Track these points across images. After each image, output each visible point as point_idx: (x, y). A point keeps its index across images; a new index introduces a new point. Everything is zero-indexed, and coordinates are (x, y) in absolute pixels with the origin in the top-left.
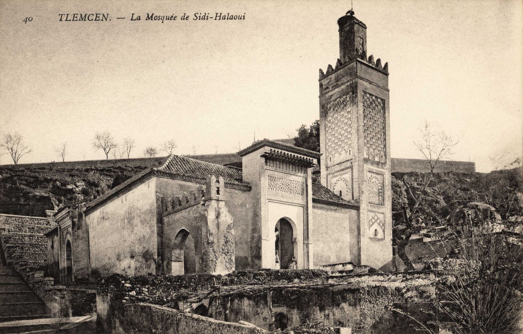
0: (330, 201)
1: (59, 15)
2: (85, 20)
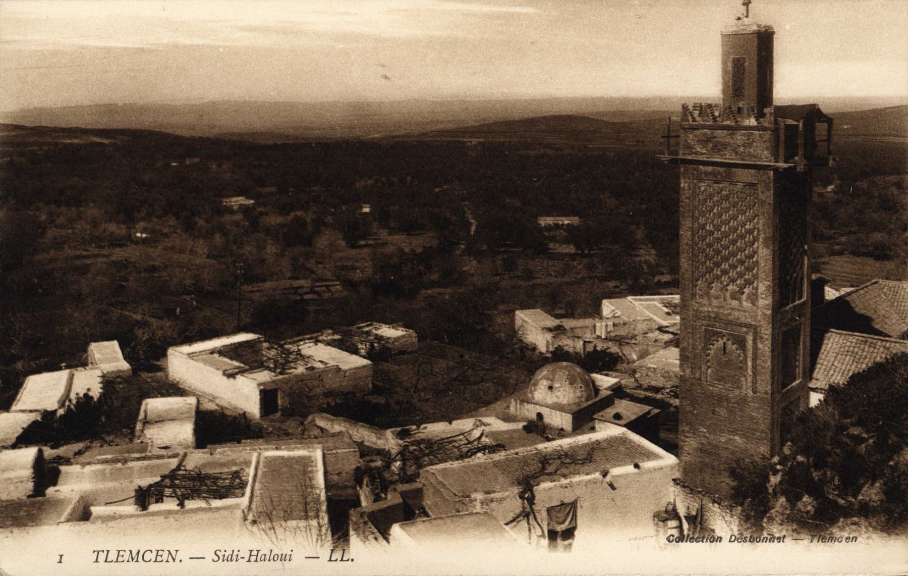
0: (305, 403)
1: (94, 551)
2: (137, 561)
